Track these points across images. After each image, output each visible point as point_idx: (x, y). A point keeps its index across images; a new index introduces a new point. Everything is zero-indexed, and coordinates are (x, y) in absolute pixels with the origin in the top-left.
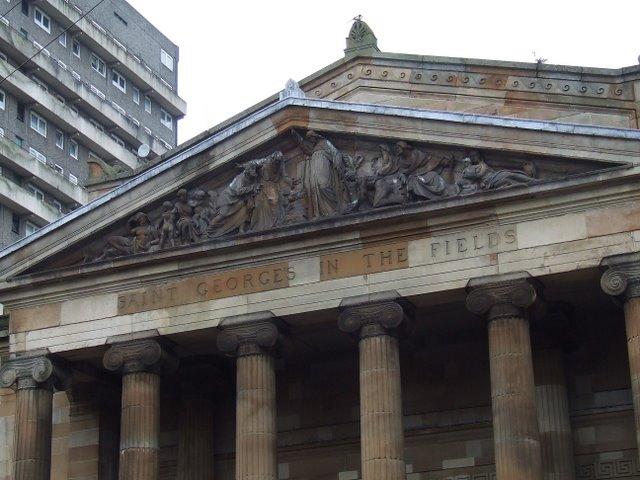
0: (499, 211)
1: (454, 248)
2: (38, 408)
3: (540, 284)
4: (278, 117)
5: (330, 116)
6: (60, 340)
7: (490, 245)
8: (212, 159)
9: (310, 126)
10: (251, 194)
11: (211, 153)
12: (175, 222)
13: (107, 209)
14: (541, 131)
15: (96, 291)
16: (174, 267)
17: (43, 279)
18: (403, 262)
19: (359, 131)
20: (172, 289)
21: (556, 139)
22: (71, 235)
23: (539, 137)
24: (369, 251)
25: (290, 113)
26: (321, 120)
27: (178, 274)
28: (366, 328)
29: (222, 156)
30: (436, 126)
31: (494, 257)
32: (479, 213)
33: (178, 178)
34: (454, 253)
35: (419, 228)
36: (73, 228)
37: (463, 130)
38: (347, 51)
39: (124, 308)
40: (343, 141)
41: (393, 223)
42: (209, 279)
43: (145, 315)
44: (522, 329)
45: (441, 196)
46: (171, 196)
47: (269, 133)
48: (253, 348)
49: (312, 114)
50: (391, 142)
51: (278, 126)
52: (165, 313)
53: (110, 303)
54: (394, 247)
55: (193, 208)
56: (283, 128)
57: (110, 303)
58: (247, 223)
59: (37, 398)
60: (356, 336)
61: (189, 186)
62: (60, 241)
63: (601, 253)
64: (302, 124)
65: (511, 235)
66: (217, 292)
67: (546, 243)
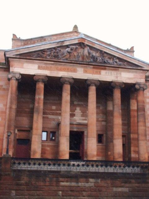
0: (120, 69)
1: (110, 73)
2: (87, 131)
3: (126, 84)
4: (80, 39)
5: (90, 42)
6: (24, 71)
7: (117, 75)
8: (64, 43)
9: (85, 43)
10: (71, 52)
11: (64, 42)
12: (53, 53)
13: (39, 47)
14: (130, 57)
15: (33, 63)
16: (53, 63)
17: (22, 57)
18: (100, 73)
19: (95, 47)
20: (51, 67)
21: (132, 59)
22: (30, 50)
23: (129, 58)
24: (93, 70)
25: (82, 39)
26: (88, 42)
27: (52, 64)
28: (92, 84)
29: (66, 43)
30: (111, 50)
31: (117, 77)
32: (116, 68)
33: (56, 45)
34: (110, 75)
35: (104, 68)
36: (30, 48)
37: (116, 53)
38: (73, 30)
39: (39, 68)
40: (91, 48)
41: (103, 66)
42: (60, 67)
43: (44, 71)
44: (120, 90)
45: (109, 63)
46: (54, 48)
47: (76, 42)
48: (68, 83)
49: (86, 41)
50: (101, 51)
51: (79, 41)
52: (49, 71)
53: (36, 66)
54: (99, 70)
55: (58, 52)
56: (80, 42)
57: (36, 66)
58: (69, 58)
59: (16, 82)
60: (89, 85)
61: (58, 47)
62: (27, 50)
63: (136, 81)
64: (83, 42)
65: (120, 74)
66: (61, 70)
67: (126, 77)
